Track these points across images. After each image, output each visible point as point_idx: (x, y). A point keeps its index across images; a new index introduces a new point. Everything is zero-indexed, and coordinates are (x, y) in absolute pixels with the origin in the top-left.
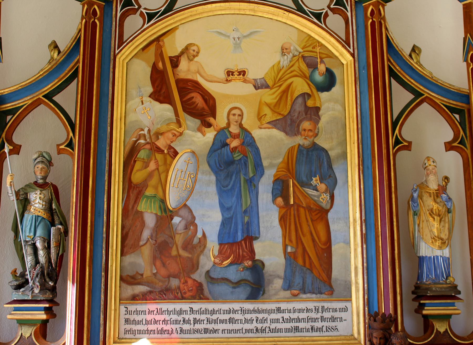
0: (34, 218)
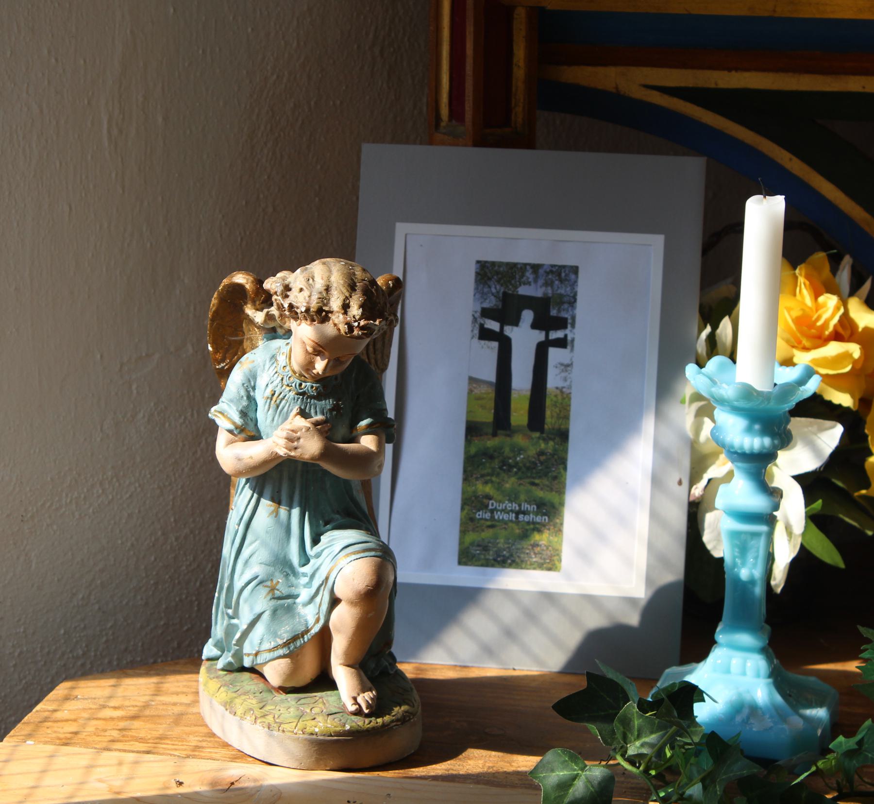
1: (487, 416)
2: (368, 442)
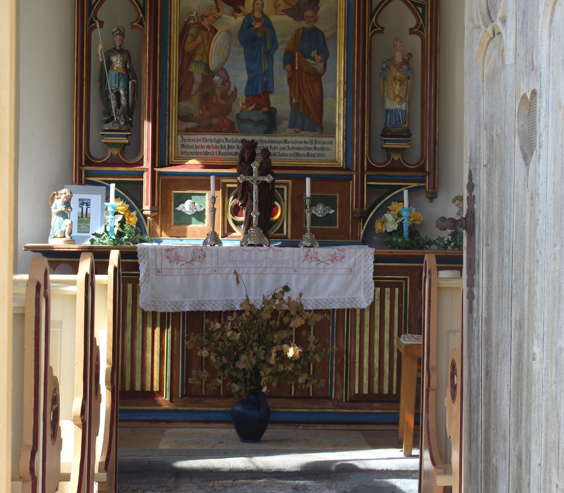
0: (117, 74)
1: (80, 216)
2: (70, 210)
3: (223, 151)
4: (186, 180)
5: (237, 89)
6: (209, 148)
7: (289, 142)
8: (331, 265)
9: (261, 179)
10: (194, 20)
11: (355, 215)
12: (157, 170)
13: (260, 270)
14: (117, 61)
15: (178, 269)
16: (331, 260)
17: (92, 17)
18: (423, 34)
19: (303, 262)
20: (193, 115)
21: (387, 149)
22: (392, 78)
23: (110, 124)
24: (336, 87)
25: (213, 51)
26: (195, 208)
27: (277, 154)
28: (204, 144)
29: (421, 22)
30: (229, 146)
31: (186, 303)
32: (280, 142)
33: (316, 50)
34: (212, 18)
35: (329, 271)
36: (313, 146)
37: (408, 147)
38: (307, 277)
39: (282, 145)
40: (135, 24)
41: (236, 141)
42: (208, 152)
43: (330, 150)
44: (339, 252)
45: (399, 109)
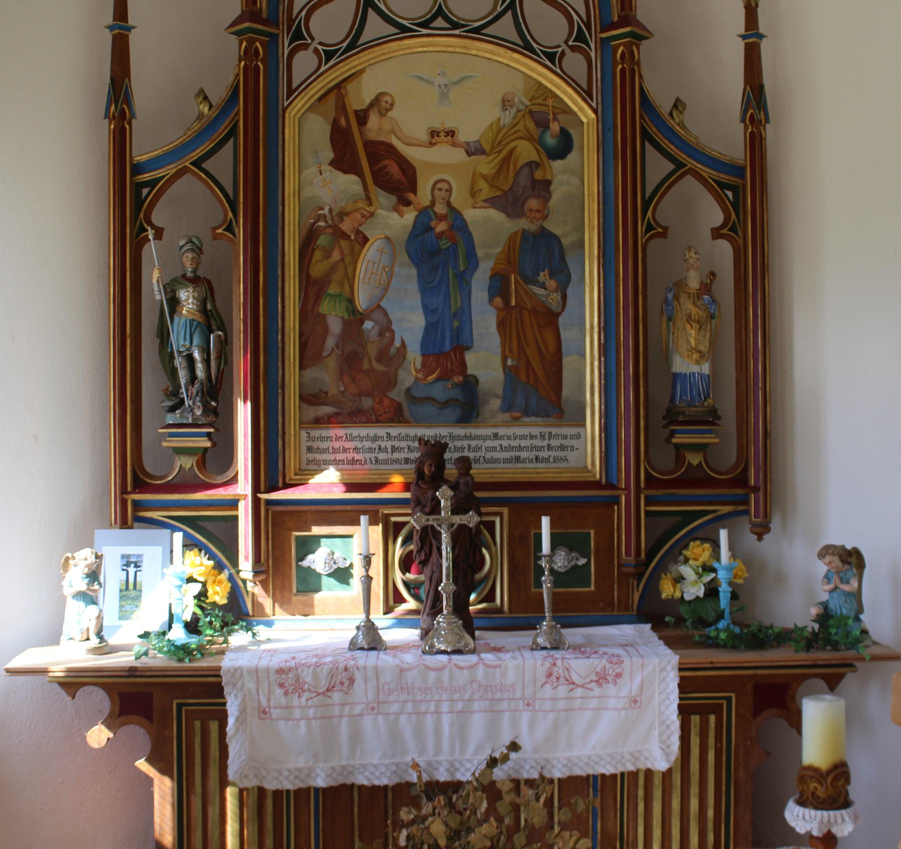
0: (188, 322)
1: (124, 587)
3: (382, 456)
4: (317, 512)
5: (407, 343)
6: (358, 453)
7: (502, 438)
8: (597, 691)
9: (457, 520)
10: (326, 222)
11: (626, 570)
12: (264, 496)
13: (460, 706)
14: (187, 297)
15: (301, 707)
16: (596, 681)
17: (141, 223)
18: (737, 238)
19: (542, 687)
20: (326, 393)
21: (676, 446)
22: (685, 318)
23: (176, 414)
24: (585, 336)
25: (362, 276)
26: (335, 563)
27: (482, 460)
28: (348, 445)
29: (733, 216)
30: (393, 447)
31: (318, 771)
32: (485, 438)
33: (546, 269)
34: (358, 216)
35: (593, 703)
36: (545, 443)
37: (717, 440)
38: (551, 716)
39: (489, 443)
40: (220, 231)
41: (407, 438)
42: (355, 459)
43: (577, 449)
44: (611, 665)
45: (698, 373)
